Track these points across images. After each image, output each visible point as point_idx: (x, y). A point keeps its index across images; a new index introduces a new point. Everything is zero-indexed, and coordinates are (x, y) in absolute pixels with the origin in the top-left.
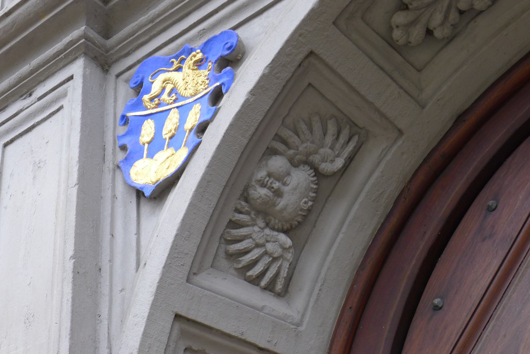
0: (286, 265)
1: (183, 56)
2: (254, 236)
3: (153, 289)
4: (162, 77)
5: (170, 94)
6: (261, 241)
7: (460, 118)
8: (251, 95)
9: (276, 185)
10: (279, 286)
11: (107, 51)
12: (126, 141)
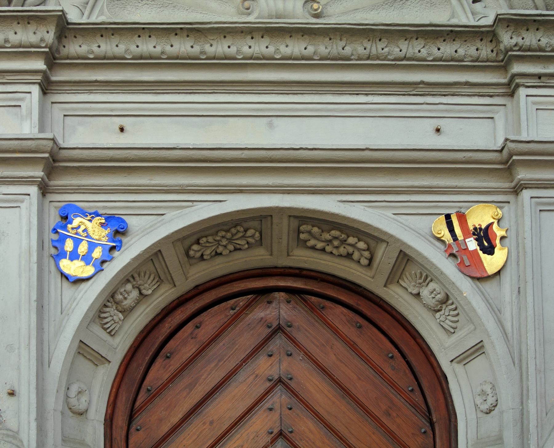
0: (119, 326)
2: (111, 312)
3: (75, 329)
6: (112, 315)
7: (197, 286)
9: (126, 296)
10: (113, 333)
11: (47, 186)
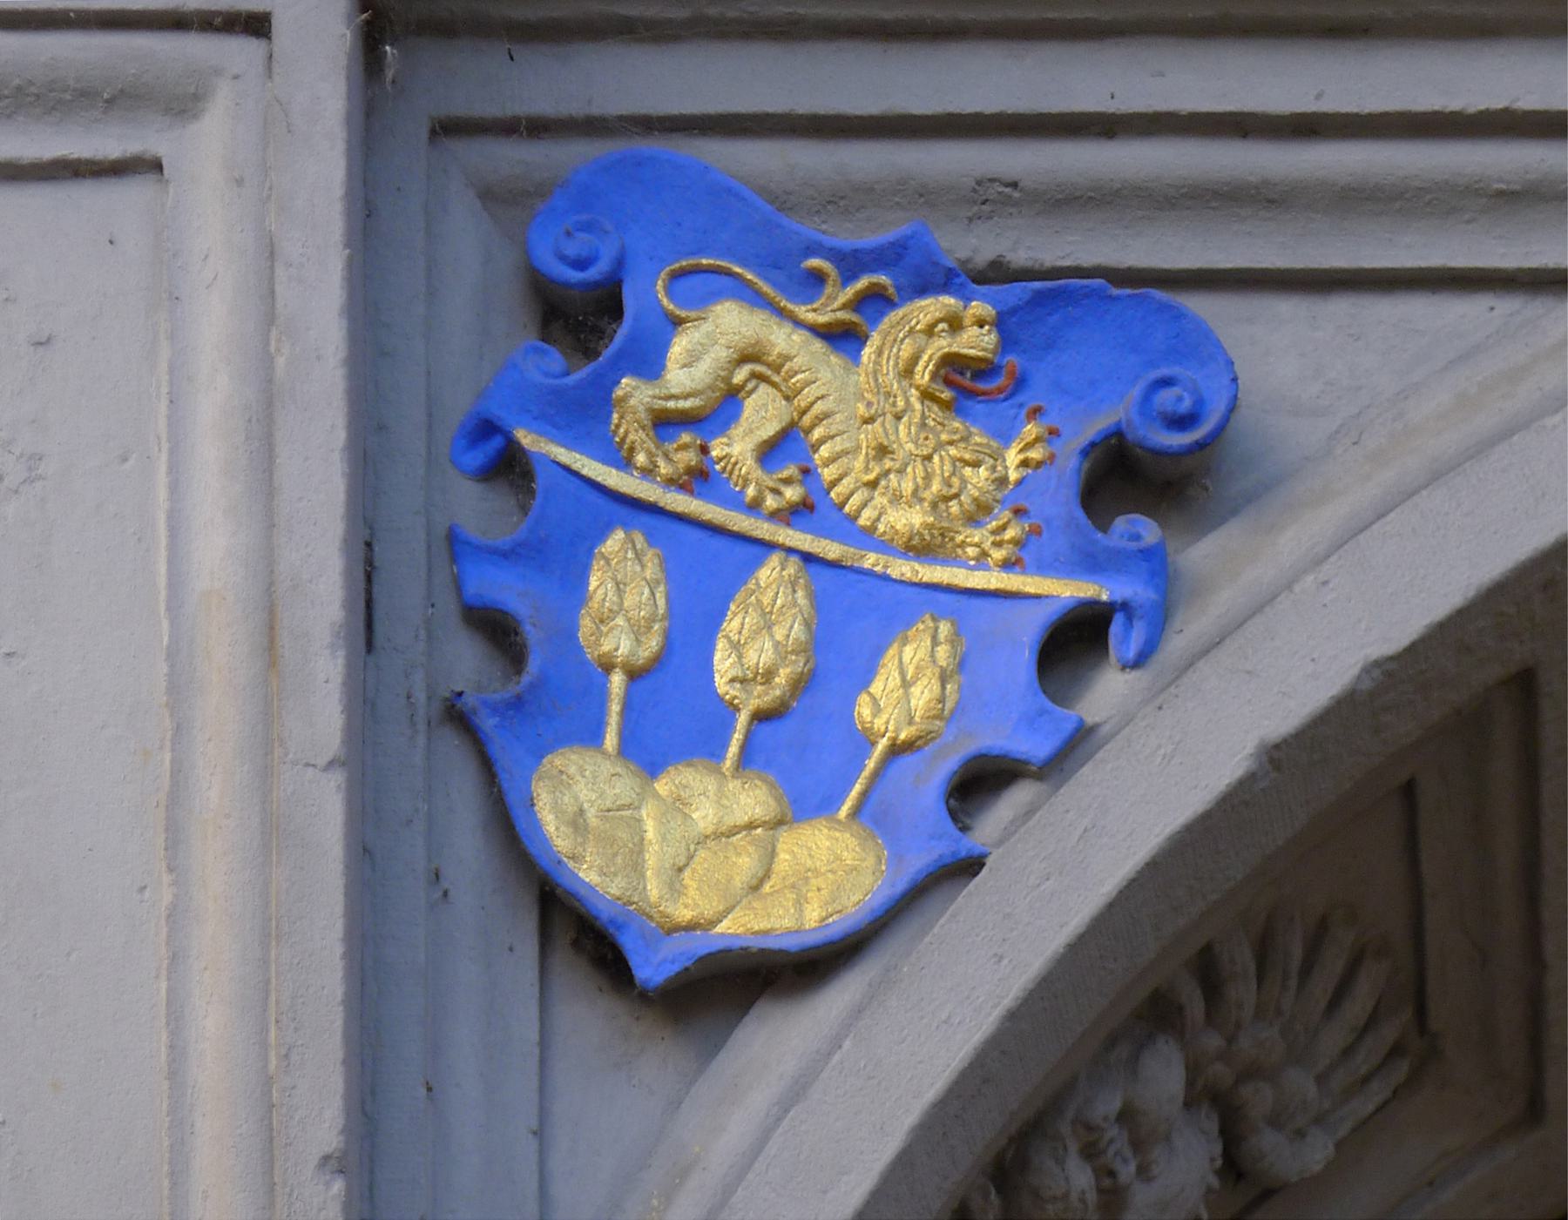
1: (883, 279)
4: (731, 322)
5: (769, 453)
8: (1272, 760)
12: (504, 588)
